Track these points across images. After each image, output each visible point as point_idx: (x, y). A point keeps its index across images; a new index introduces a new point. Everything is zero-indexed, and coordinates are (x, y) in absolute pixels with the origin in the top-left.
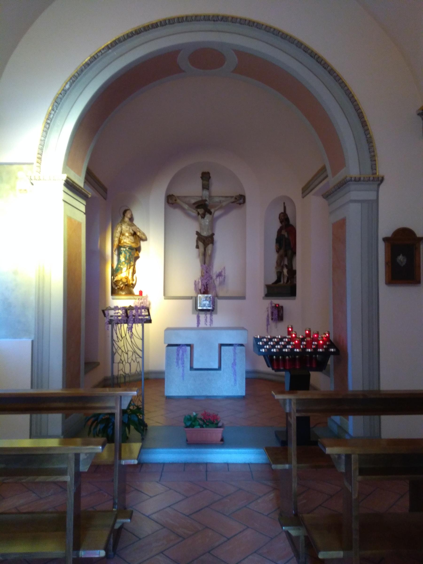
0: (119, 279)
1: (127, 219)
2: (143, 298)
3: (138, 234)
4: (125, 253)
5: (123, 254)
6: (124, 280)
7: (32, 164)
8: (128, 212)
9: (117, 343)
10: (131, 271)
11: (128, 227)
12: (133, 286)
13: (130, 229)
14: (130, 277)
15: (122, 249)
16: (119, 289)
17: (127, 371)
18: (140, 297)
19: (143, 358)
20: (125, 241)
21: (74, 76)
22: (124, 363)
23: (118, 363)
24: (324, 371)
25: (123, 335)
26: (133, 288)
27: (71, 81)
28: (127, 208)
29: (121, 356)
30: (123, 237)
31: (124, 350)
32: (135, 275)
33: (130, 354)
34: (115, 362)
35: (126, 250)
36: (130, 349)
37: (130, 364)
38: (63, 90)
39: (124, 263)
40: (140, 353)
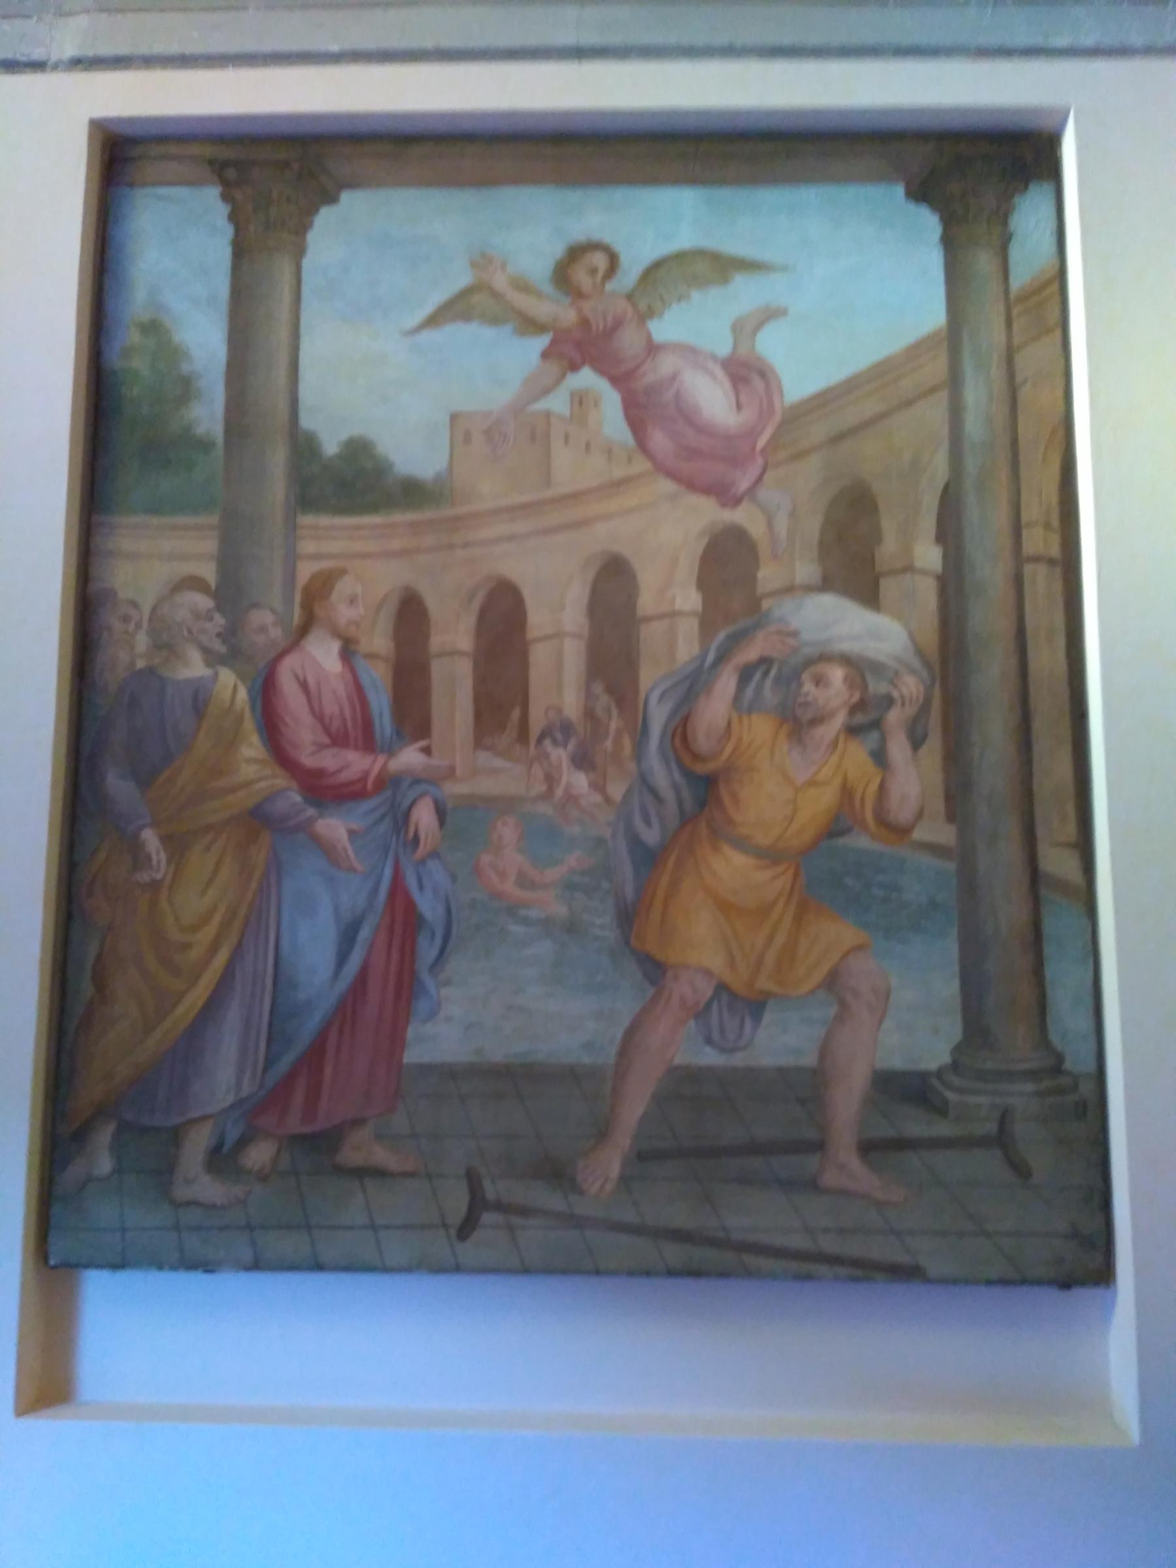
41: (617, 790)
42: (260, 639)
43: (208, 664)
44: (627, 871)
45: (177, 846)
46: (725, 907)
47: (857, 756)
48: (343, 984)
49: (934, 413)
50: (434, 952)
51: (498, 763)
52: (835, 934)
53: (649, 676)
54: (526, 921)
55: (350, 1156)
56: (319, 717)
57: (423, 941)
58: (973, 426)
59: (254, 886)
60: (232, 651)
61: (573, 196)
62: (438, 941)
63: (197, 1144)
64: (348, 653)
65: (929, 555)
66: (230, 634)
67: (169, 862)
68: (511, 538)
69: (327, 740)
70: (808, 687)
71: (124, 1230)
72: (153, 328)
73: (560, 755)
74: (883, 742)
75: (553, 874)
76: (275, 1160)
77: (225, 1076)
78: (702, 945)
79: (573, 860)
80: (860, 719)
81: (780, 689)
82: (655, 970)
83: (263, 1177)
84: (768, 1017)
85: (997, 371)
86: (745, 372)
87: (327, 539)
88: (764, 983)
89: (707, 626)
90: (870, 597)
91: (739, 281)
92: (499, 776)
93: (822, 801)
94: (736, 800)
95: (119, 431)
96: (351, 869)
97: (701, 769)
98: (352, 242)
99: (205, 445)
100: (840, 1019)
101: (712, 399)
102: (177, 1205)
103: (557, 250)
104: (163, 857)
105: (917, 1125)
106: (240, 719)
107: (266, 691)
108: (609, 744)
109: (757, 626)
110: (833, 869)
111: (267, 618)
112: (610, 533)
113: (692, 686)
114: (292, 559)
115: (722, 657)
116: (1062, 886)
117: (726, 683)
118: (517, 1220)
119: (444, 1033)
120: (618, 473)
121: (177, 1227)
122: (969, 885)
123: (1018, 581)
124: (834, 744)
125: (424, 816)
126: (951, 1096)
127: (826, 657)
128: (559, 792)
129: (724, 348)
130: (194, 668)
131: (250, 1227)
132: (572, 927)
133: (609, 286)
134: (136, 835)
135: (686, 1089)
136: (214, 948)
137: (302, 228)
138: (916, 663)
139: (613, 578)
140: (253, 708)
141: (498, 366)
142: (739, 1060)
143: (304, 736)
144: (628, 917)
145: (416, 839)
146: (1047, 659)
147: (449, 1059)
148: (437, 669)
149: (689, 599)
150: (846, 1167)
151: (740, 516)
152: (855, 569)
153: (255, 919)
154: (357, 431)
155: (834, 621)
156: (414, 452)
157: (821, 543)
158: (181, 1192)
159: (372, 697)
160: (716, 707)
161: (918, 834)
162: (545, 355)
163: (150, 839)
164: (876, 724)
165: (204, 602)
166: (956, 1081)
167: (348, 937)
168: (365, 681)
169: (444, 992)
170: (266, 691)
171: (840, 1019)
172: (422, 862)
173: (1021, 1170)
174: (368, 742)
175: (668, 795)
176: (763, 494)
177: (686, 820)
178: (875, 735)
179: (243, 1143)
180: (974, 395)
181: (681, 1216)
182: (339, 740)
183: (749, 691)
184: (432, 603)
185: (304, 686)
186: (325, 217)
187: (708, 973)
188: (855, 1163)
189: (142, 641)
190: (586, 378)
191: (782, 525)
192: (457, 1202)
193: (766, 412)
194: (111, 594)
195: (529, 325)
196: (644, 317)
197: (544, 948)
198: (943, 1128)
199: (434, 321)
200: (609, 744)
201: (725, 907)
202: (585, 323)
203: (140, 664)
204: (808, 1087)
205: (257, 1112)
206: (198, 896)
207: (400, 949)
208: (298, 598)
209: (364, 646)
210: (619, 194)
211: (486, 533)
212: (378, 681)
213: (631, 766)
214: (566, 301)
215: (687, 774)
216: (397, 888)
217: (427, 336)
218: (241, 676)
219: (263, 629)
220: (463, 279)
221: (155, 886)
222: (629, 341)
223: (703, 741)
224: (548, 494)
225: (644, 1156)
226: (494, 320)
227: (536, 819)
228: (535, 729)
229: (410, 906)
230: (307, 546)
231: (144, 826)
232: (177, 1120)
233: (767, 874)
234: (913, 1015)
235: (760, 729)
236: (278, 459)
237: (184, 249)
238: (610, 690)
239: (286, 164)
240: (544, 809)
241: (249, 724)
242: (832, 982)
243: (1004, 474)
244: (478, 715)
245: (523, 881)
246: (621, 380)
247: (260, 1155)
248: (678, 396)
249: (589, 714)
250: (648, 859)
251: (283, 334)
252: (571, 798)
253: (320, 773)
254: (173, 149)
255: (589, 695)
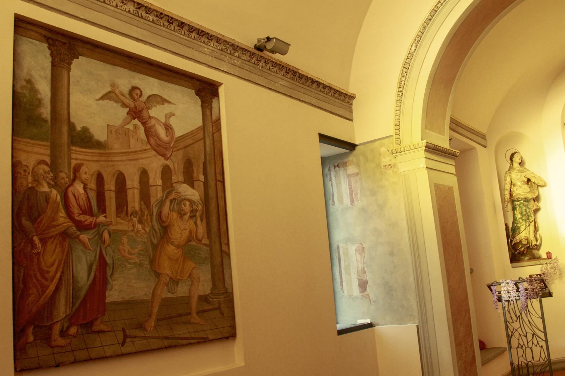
0: (518, 241)
1: (516, 165)
2: (552, 262)
3: (533, 180)
4: (520, 207)
5: (518, 208)
6: (525, 242)
7: (392, 136)
8: (516, 155)
9: (512, 324)
10: (532, 228)
11: (519, 174)
12: (538, 247)
13: (521, 176)
14: (532, 237)
15: (515, 203)
16: (519, 253)
17: (529, 358)
18: (548, 261)
19: (546, 341)
20: (518, 192)
21: (418, 36)
22: (524, 348)
23: (517, 348)
24: (537, 355)
25: (518, 314)
26: (538, 250)
27: (416, 42)
28: (513, 151)
29: (519, 340)
30: (515, 188)
31: (521, 333)
32: (538, 233)
33: (530, 336)
34: (512, 346)
35: (521, 203)
36: (528, 330)
37: (531, 349)
38: (409, 53)
39: (520, 220)
40: (542, 335)
41: (147, 230)
42: (63, 181)
43: (49, 188)
44: (151, 250)
45: (44, 241)
46: (170, 259)
47: (192, 222)
48: (90, 282)
49: (201, 144)
50: (111, 272)
51: (122, 221)
52: (190, 264)
53: (153, 200)
54: (130, 263)
55: (95, 328)
56: (79, 205)
57: (108, 268)
58: (208, 149)
59: (65, 254)
60: (55, 184)
61: (133, 74)
62: (111, 269)
63: (57, 329)
64: (85, 188)
65: (202, 178)
66: (55, 179)
67: (42, 247)
68: (122, 161)
69: (81, 212)
70: (183, 206)
71: (38, 357)
72: (29, 82)
73: (135, 220)
74: (196, 220)
75: (136, 251)
76: (77, 332)
77: (62, 310)
78: (166, 268)
79: (140, 247)
80: (192, 214)
81: (179, 201)
82: (158, 275)
83: (74, 337)
84: (179, 285)
85: (211, 138)
86: (168, 128)
87: (79, 155)
88: (178, 277)
89: (163, 190)
90: (192, 186)
91: (166, 104)
92: (122, 225)
93: (187, 233)
94: (170, 232)
95: (23, 112)
96: (90, 249)
97: (164, 225)
98: (81, 68)
99: (45, 121)
100: (192, 284)
101: (162, 132)
102: (53, 347)
103: (130, 87)
104: (40, 245)
105: (206, 307)
106: (59, 205)
107: (65, 197)
108: (145, 217)
109: (173, 190)
110: (188, 250)
111: (65, 176)
112: (143, 163)
113: (161, 203)
114: (70, 159)
115: (167, 198)
116: (226, 252)
117: (168, 204)
118: (134, 339)
119: (113, 295)
120: (144, 148)
121: (53, 354)
122: (212, 255)
123: (216, 185)
124: (188, 220)
125: (106, 235)
126: (211, 300)
127: (185, 199)
128: (136, 229)
129: (164, 121)
130: (45, 188)
131: (72, 351)
132: (141, 265)
133: (141, 99)
134: (32, 238)
135: (166, 303)
136: (56, 272)
137: (70, 64)
138: (201, 202)
139: (144, 174)
140: (62, 202)
141: (118, 114)
142: (175, 295)
143: (76, 210)
144: (152, 262)
145: (105, 242)
146: (221, 203)
147: (116, 300)
148: (107, 194)
149: (160, 182)
150: (195, 318)
151: (168, 162)
152: (190, 181)
153: (66, 263)
154: (85, 125)
155: (186, 190)
156: (100, 135)
157: (183, 172)
158: (54, 344)
159: (92, 201)
160: (166, 210)
161: (203, 242)
162: (128, 114)
163: (36, 239)
164: (195, 216)
165: (47, 169)
166: (211, 296)
167: (90, 268)
168: (90, 196)
169: (114, 283)
170: (65, 197)
171: (192, 284)
172: (106, 248)
173: (222, 314)
174: (92, 215)
175: (158, 231)
176: (172, 158)
177: (162, 237)
178: (195, 218)
179: (68, 328)
180: (208, 142)
181: (166, 333)
182: (84, 212)
183: (172, 207)
184: (105, 176)
185: (75, 196)
186: (75, 61)
187: (168, 275)
188: (196, 316)
189: (30, 179)
190: (136, 121)
191: (176, 165)
192: (121, 337)
193: (172, 138)
194: (20, 162)
195: (124, 105)
196: (148, 109)
197: (135, 270)
198: (211, 307)
199: (102, 98)
200: (145, 217)
201: (170, 259)
202: (136, 107)
203: (30, 185)
204: (187, 300)
205: (72, 319)
206: (51, 257)
207: (102, 272)
208: (72, 171)
209: (89, 186)
210: (142, 76)
211: (116, 159)
212: (93, 196)
213: (150, 223)
214: (132, 100)
215: (161, 226)
216: (101, 255)
217: (101, 101)
218: (58, 192)
219: (63, 179)
220: (109, 89)
221: (38, 254)
222: (145, 113)
223: (164, 219)
224: (130, 150)
225: (158, 320)
226: (116, 102)
227: (130, 236)
228: (130, 212)
229: (104, 260)
230: (73, 156)
231: (33, 236)
232: (50, 323)
233: (176, 251)
234: (204, 286)
235: (174, 215)
236: (65, 129)
237: (39, 59)
238: (145, 203)
239: (65, 43)
240: (133, 234)
241: (61, 207)
242: (190, 276)
243: (213, 161)
244: (117, 208)
245: (130, 253)
246: (144, 124)
247: (73, 330)
248: (155, 130)
249: (141, 210)
250: (155, 247)
251: (65, 93)
252: (138, 231)
253: (80, 222)
254: (34, 28)
255: (141, 205)
